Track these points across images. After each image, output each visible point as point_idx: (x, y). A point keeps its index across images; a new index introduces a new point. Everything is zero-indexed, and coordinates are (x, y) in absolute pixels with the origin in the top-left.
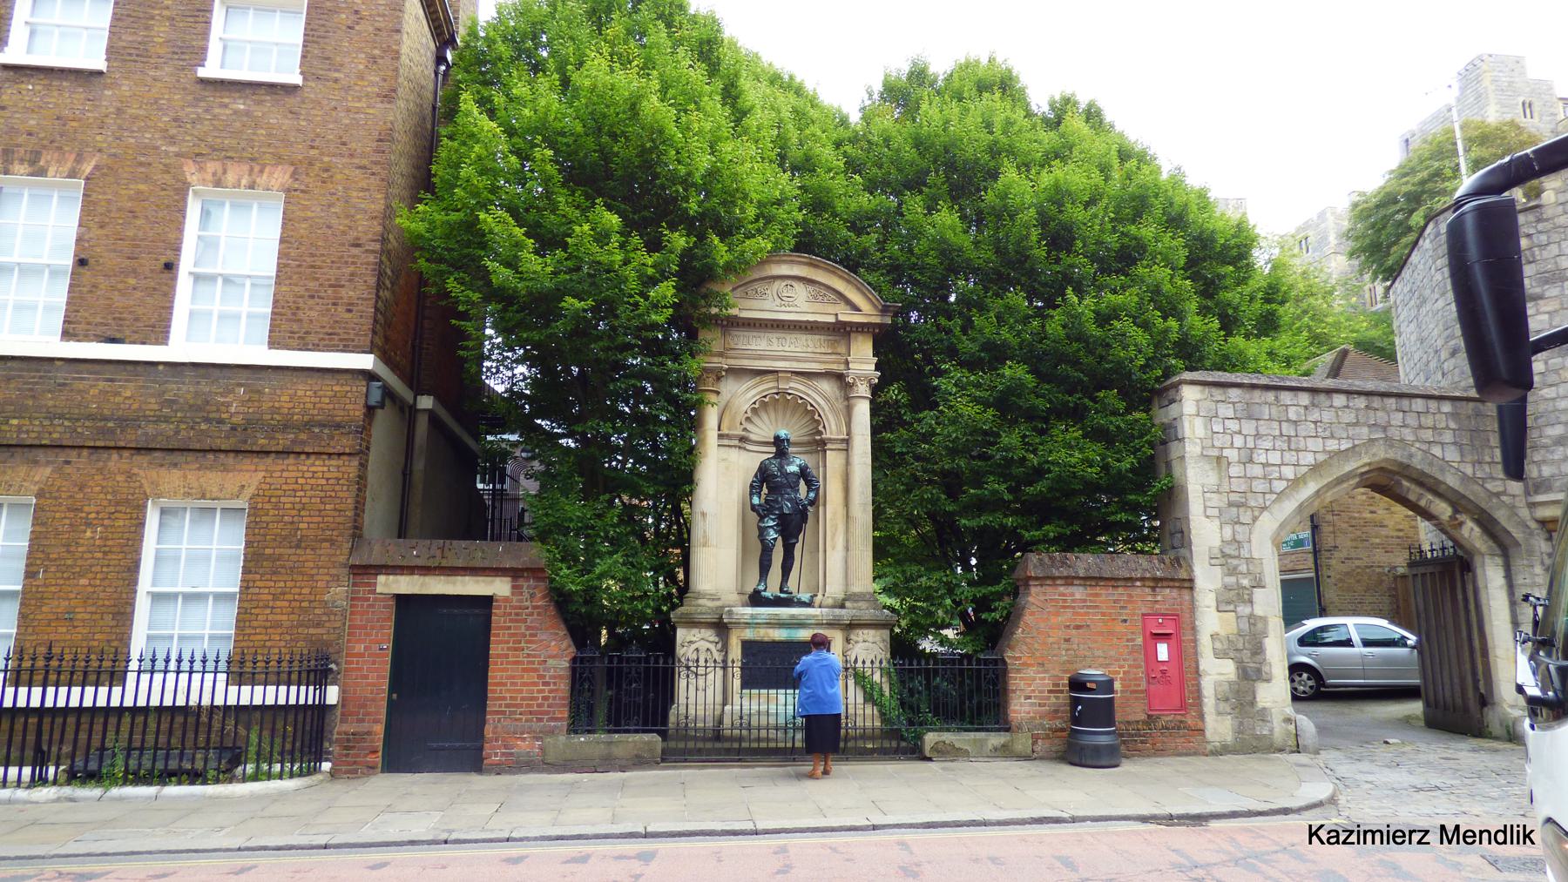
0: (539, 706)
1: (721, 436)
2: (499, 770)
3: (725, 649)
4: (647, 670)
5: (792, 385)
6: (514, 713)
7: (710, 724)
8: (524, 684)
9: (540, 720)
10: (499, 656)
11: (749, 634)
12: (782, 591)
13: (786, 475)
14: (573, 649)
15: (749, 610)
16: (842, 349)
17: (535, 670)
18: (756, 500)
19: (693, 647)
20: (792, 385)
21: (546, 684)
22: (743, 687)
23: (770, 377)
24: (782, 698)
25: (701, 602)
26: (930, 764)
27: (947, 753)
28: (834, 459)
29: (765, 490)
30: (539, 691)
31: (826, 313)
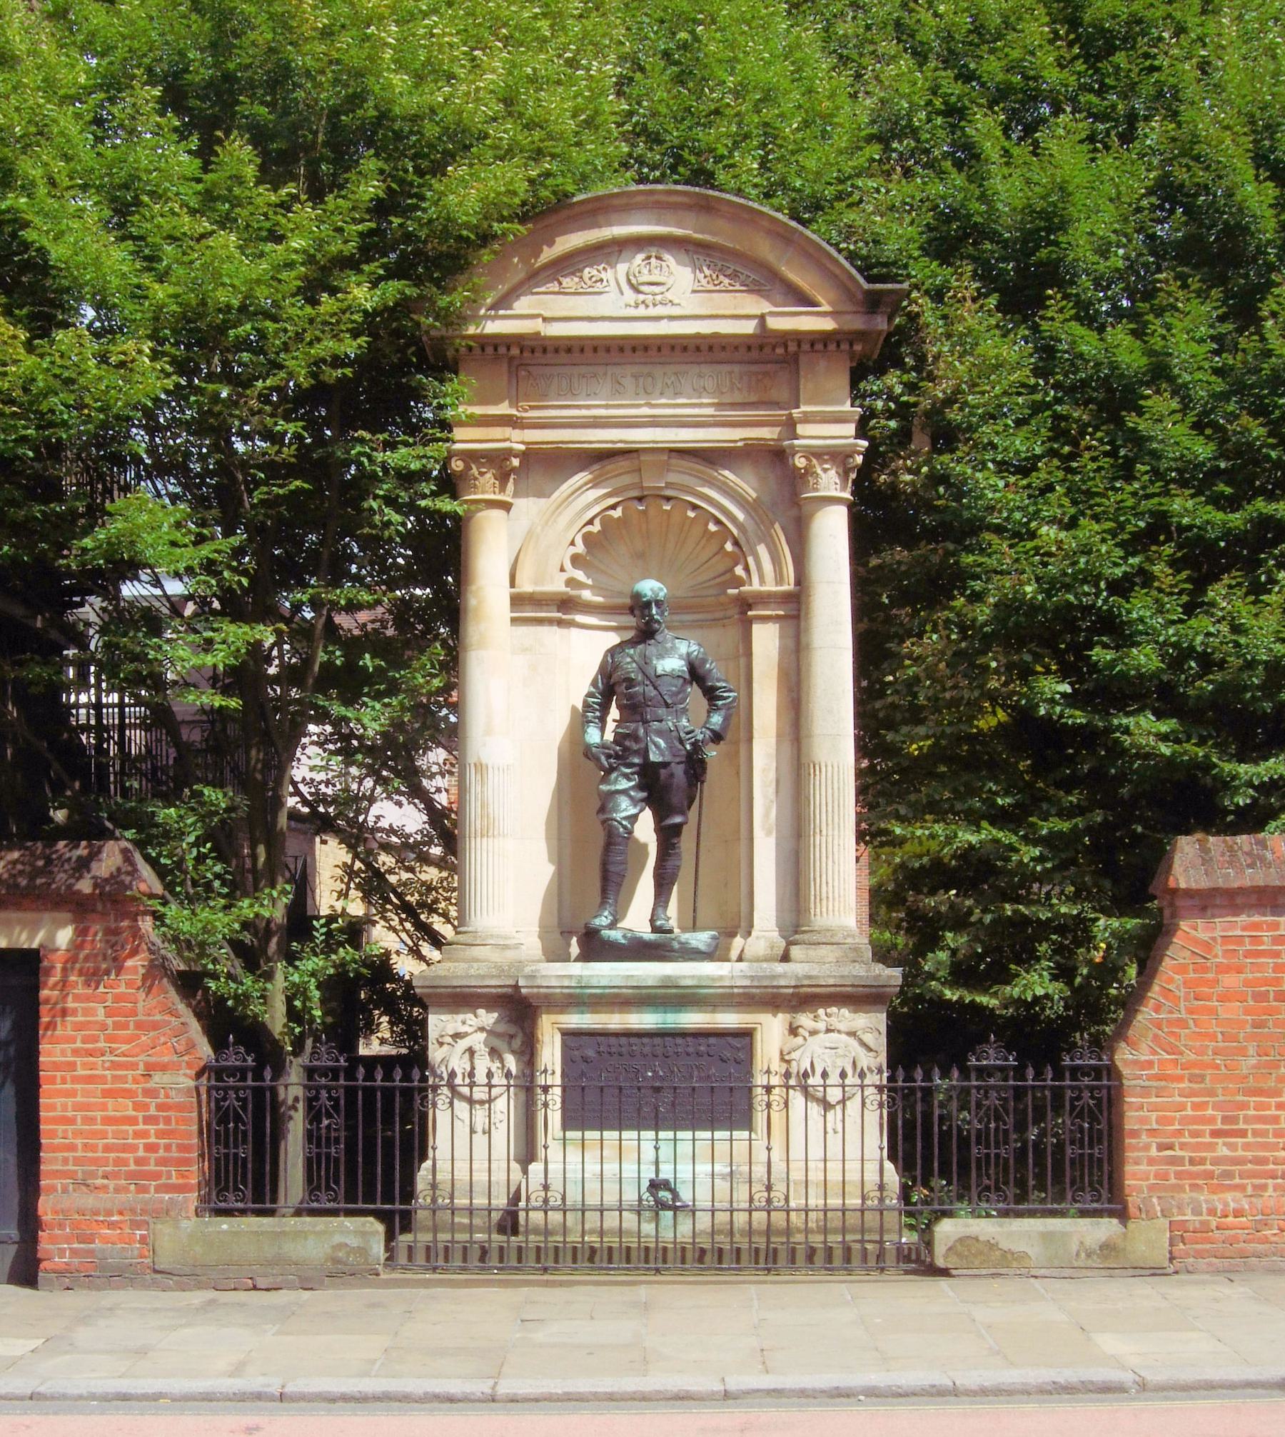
0: (138, 1162)
1: (518, 601)
2: (72, 1279)
3: (528, 1052)
4: (351, 1092)
5: (673, 477)
6: (93, 1175)
7: (501, 1201)
8: (108, 1121)
9: (143, 1189)
10: (57, 1066)
11: (576, 1020)
12: (655, 930)
13: (654, 679)
14: (205, 1050)
15: (578, 969)
16: (783, 394)
17: (128, 1094)
18: (593, 735)
19: (463, 1044)
20: (673, 477)
21: (148, 1120)
22: (566, 1126)
23: (623, 464)
24: (723, 1148)
25: (476, 952)
26: (943, 1283)
27: (998, 1264)
28: (766, 640)
29: (614, 713)
30: (137, 1135)
31: (734, 312)
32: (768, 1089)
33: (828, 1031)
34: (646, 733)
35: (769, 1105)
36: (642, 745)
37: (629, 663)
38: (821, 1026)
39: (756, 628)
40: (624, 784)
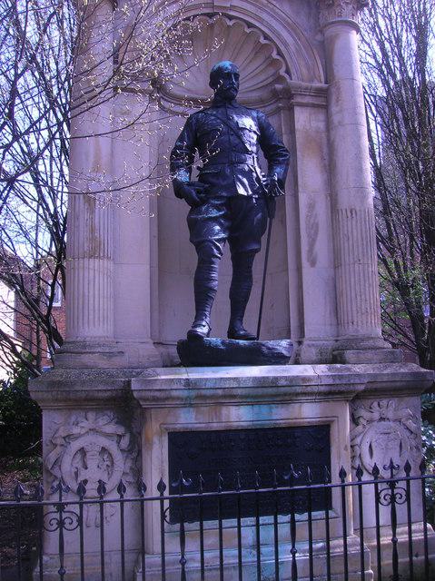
11: (187, 419)
25: (86, 359)
32: (61, 507)
33: (382, 419)
34: (232, 172)
35: (61, 524)
36: (230, 181)
37: (213, 118)
38: (376, 415)
39: (297, 111)
40: (214, 213)
